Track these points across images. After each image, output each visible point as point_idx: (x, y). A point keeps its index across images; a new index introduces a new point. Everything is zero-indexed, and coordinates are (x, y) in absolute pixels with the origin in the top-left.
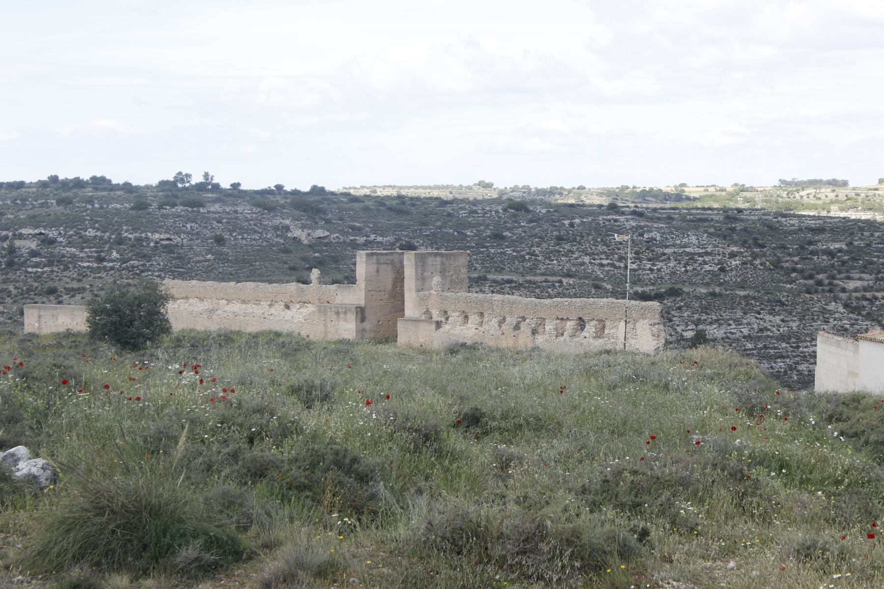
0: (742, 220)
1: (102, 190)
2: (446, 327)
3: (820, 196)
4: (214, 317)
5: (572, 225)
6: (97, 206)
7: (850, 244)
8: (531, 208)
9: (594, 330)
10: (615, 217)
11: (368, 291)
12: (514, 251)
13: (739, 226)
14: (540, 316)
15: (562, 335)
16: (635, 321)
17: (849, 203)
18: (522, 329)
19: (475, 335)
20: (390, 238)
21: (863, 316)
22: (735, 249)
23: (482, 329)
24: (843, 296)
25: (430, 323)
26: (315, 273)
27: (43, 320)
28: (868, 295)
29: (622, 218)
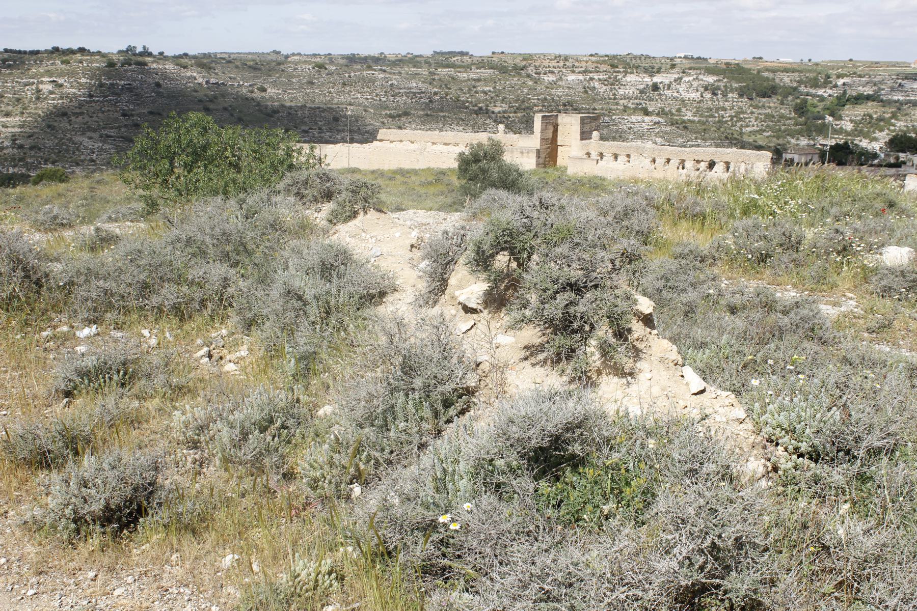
0: (438, 74)
5: (350, 77)
7: (494, 88)
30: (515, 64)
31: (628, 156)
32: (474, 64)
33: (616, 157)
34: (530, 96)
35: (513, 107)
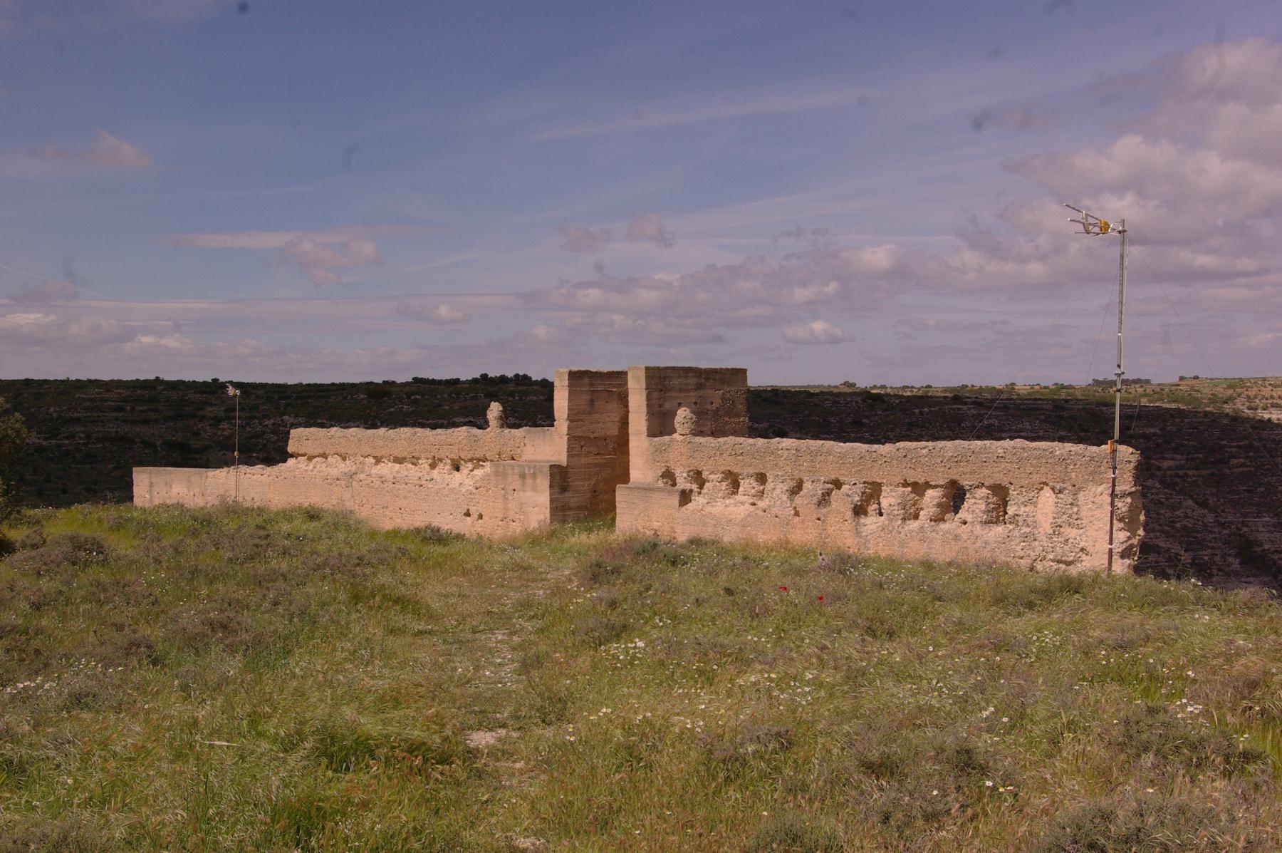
0: (1068, 409)
1: (522, 385)
2: (698, 501)
3: (1130, 390)
4: (354, 483)
5: (921, 413)
6: (517, 398)
7: (1163, 429)
8: (886, 399)
9: (983, 507)
10: (958, 406)
11: (573, 439)
12: (872, 436)
13: (1066, 414)
14: (870, 480)
15: (916, 517)
16: (1076, 489)
17: (1156, 396)
18: (834, 505)
19: (749, 515)
20: (765, 425)
21: (1176, 491)
22: (1063, 433)
23: (761, 504)
24: (1159, 473)
25: (670, 493)
26: (495, 409)
27: (155, 489)
28: (1181, 473)
29: (965, 407)
30: (1213, 394)
31: (762, 479)
32: (1146, 395)
33: (733, 481)
34: (1224, 442)
35: (1193, 459)
